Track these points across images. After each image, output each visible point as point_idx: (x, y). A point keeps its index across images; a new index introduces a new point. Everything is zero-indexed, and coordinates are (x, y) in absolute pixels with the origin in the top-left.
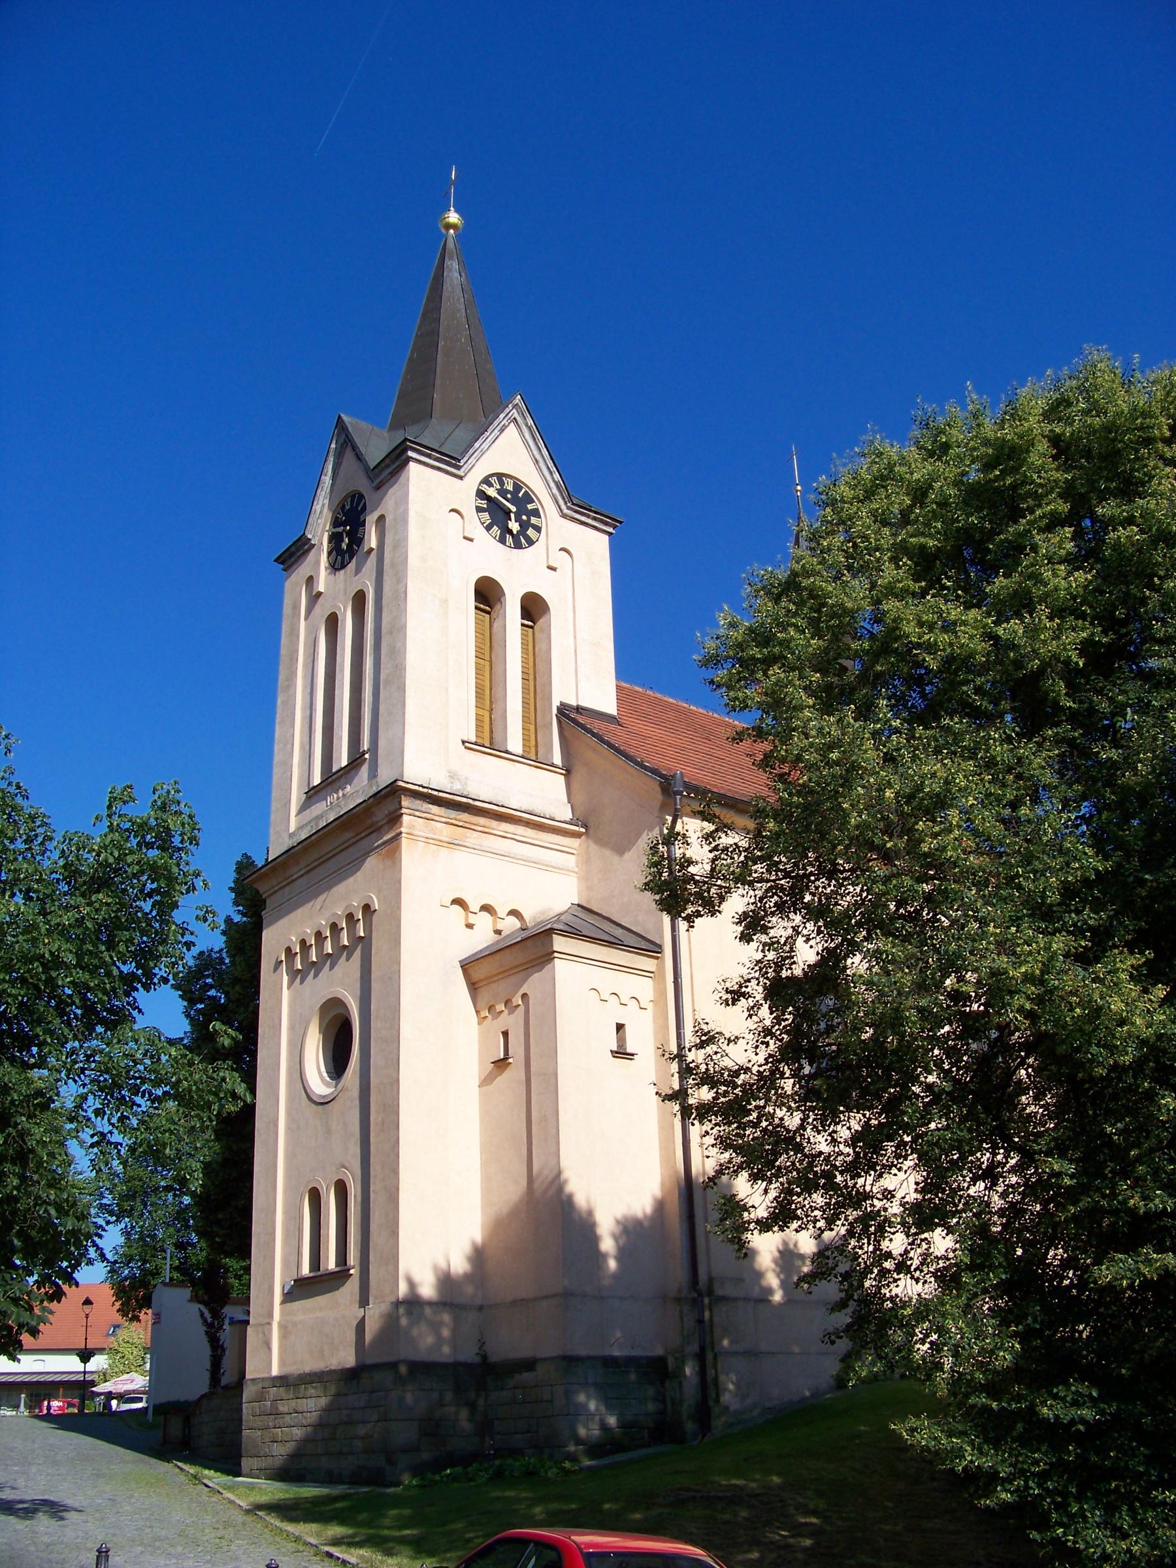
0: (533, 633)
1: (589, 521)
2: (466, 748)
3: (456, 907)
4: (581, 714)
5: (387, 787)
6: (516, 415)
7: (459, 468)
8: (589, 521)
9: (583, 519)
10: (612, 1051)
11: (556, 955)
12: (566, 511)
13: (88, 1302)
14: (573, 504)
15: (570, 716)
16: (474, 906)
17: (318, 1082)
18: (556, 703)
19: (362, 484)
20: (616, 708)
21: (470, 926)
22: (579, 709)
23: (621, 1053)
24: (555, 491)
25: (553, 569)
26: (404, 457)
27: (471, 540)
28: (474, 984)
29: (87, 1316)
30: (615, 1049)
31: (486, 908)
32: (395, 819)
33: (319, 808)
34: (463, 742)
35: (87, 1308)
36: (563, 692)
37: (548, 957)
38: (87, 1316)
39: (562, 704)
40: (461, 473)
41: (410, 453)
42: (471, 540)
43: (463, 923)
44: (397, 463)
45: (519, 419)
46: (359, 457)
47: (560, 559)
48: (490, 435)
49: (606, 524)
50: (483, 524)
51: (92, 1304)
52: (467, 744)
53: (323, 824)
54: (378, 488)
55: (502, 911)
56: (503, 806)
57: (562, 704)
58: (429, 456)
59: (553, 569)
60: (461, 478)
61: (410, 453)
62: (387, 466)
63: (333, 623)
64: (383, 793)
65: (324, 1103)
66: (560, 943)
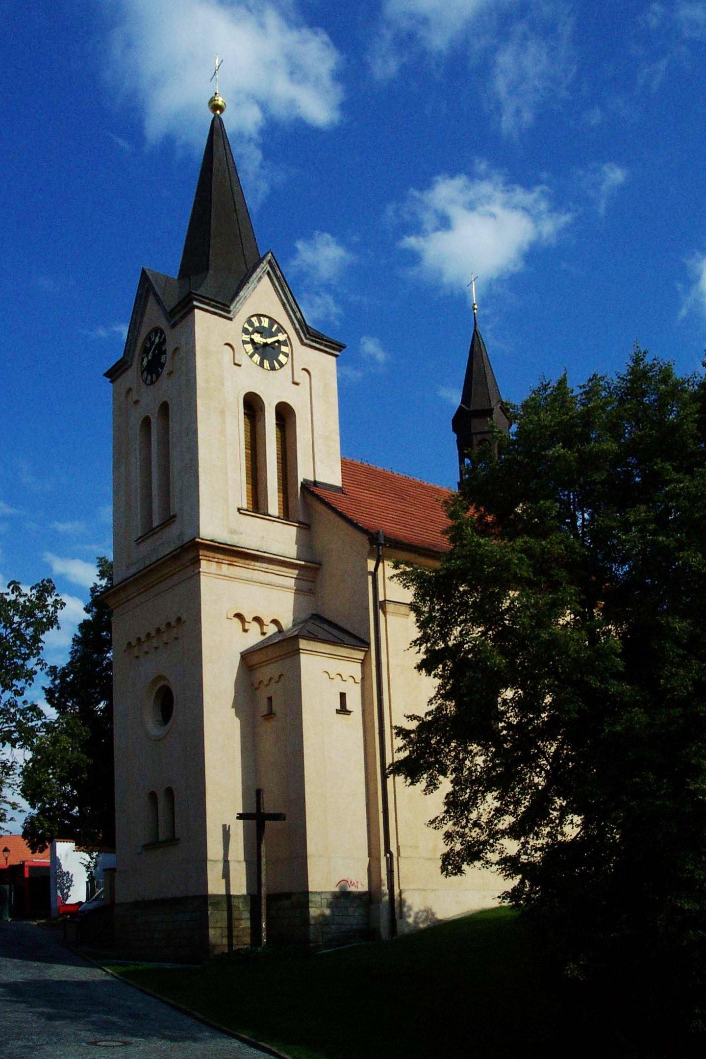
0: (293, 378)
1: (322, 347)
2: (240, 513)
3: (236, 620)
4: (318, 487)
5: (188, 542)
6: (269, 269)
7: (229, 312)
8: (322, 347)
9: (317, 346)
10: (337, 710)
11: (301, 651)
12: (305, 341)
13: (6, 850)
14: (310, 335)
15: (311, 488)
16: (249, 617)
17: (153, 728)
18: (300, 480)
19: (163, 324)
20: (341, 482)
21: (245, 631)
22: (315, 483)
23: (343, 710)
24: (298, 326)
25: (297, 384)
26: (190, 305)
27: (239, 365)
28: (250, 667)
29: (6, 859)
30: (339, 708)
31: (257, 619)
32: (197, 562)
33: (145, 548)
34: (239, 509)
35: (6, 854)
36: (304, 473)
37: (297, 652)
38: (6, 859)
39: (304, 480)
40: (230, 316)
41: (195, 303)
42: (239, 365)
43: (291, 382)
44: (187, 309)
45: (271, 272)
46: (159, 302)
47: (301, 376)
48: (250, 286)
49: (334, 349)
50: (247, 353)
51: (9, 851)
52: (241, 511)
53: (148, 563)
54: (173, 326)
55: (267, 620)
56: (265, 552)
57: (304, 480)
58: (208, 304)
59: (297, 384)
60: (231, 319)
61: (195, 303)
62: (179, 311)
63: (147, 422)
64: (186, 546)
65: (158, 740)
66: (303, 644)
